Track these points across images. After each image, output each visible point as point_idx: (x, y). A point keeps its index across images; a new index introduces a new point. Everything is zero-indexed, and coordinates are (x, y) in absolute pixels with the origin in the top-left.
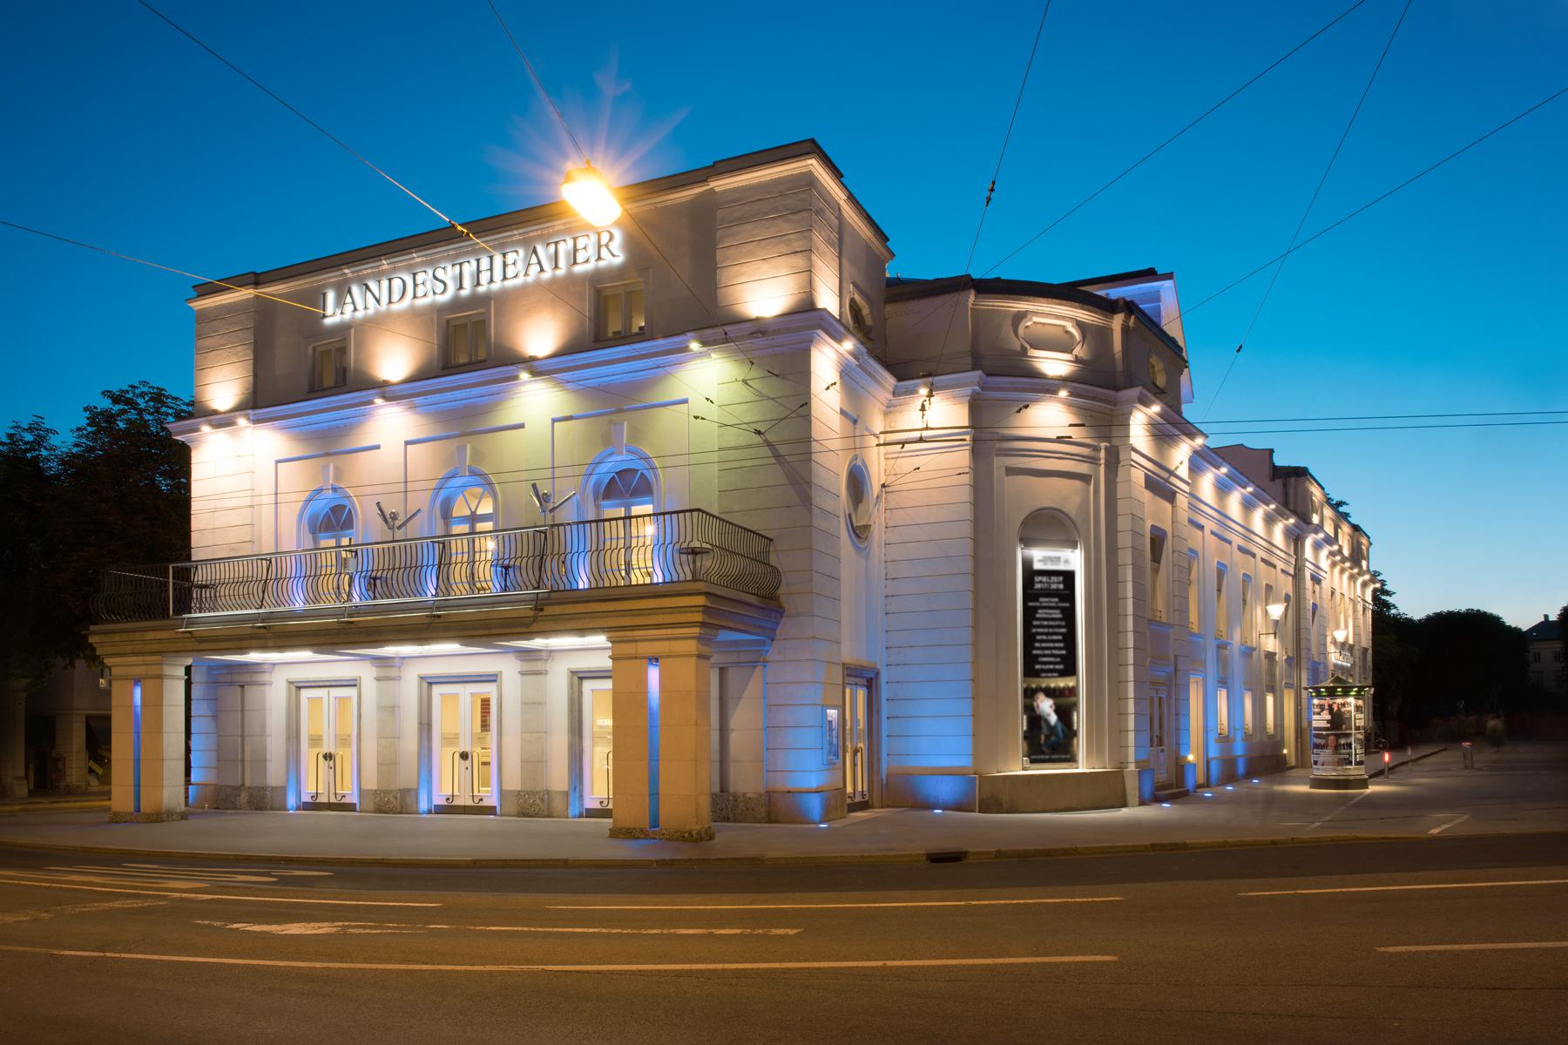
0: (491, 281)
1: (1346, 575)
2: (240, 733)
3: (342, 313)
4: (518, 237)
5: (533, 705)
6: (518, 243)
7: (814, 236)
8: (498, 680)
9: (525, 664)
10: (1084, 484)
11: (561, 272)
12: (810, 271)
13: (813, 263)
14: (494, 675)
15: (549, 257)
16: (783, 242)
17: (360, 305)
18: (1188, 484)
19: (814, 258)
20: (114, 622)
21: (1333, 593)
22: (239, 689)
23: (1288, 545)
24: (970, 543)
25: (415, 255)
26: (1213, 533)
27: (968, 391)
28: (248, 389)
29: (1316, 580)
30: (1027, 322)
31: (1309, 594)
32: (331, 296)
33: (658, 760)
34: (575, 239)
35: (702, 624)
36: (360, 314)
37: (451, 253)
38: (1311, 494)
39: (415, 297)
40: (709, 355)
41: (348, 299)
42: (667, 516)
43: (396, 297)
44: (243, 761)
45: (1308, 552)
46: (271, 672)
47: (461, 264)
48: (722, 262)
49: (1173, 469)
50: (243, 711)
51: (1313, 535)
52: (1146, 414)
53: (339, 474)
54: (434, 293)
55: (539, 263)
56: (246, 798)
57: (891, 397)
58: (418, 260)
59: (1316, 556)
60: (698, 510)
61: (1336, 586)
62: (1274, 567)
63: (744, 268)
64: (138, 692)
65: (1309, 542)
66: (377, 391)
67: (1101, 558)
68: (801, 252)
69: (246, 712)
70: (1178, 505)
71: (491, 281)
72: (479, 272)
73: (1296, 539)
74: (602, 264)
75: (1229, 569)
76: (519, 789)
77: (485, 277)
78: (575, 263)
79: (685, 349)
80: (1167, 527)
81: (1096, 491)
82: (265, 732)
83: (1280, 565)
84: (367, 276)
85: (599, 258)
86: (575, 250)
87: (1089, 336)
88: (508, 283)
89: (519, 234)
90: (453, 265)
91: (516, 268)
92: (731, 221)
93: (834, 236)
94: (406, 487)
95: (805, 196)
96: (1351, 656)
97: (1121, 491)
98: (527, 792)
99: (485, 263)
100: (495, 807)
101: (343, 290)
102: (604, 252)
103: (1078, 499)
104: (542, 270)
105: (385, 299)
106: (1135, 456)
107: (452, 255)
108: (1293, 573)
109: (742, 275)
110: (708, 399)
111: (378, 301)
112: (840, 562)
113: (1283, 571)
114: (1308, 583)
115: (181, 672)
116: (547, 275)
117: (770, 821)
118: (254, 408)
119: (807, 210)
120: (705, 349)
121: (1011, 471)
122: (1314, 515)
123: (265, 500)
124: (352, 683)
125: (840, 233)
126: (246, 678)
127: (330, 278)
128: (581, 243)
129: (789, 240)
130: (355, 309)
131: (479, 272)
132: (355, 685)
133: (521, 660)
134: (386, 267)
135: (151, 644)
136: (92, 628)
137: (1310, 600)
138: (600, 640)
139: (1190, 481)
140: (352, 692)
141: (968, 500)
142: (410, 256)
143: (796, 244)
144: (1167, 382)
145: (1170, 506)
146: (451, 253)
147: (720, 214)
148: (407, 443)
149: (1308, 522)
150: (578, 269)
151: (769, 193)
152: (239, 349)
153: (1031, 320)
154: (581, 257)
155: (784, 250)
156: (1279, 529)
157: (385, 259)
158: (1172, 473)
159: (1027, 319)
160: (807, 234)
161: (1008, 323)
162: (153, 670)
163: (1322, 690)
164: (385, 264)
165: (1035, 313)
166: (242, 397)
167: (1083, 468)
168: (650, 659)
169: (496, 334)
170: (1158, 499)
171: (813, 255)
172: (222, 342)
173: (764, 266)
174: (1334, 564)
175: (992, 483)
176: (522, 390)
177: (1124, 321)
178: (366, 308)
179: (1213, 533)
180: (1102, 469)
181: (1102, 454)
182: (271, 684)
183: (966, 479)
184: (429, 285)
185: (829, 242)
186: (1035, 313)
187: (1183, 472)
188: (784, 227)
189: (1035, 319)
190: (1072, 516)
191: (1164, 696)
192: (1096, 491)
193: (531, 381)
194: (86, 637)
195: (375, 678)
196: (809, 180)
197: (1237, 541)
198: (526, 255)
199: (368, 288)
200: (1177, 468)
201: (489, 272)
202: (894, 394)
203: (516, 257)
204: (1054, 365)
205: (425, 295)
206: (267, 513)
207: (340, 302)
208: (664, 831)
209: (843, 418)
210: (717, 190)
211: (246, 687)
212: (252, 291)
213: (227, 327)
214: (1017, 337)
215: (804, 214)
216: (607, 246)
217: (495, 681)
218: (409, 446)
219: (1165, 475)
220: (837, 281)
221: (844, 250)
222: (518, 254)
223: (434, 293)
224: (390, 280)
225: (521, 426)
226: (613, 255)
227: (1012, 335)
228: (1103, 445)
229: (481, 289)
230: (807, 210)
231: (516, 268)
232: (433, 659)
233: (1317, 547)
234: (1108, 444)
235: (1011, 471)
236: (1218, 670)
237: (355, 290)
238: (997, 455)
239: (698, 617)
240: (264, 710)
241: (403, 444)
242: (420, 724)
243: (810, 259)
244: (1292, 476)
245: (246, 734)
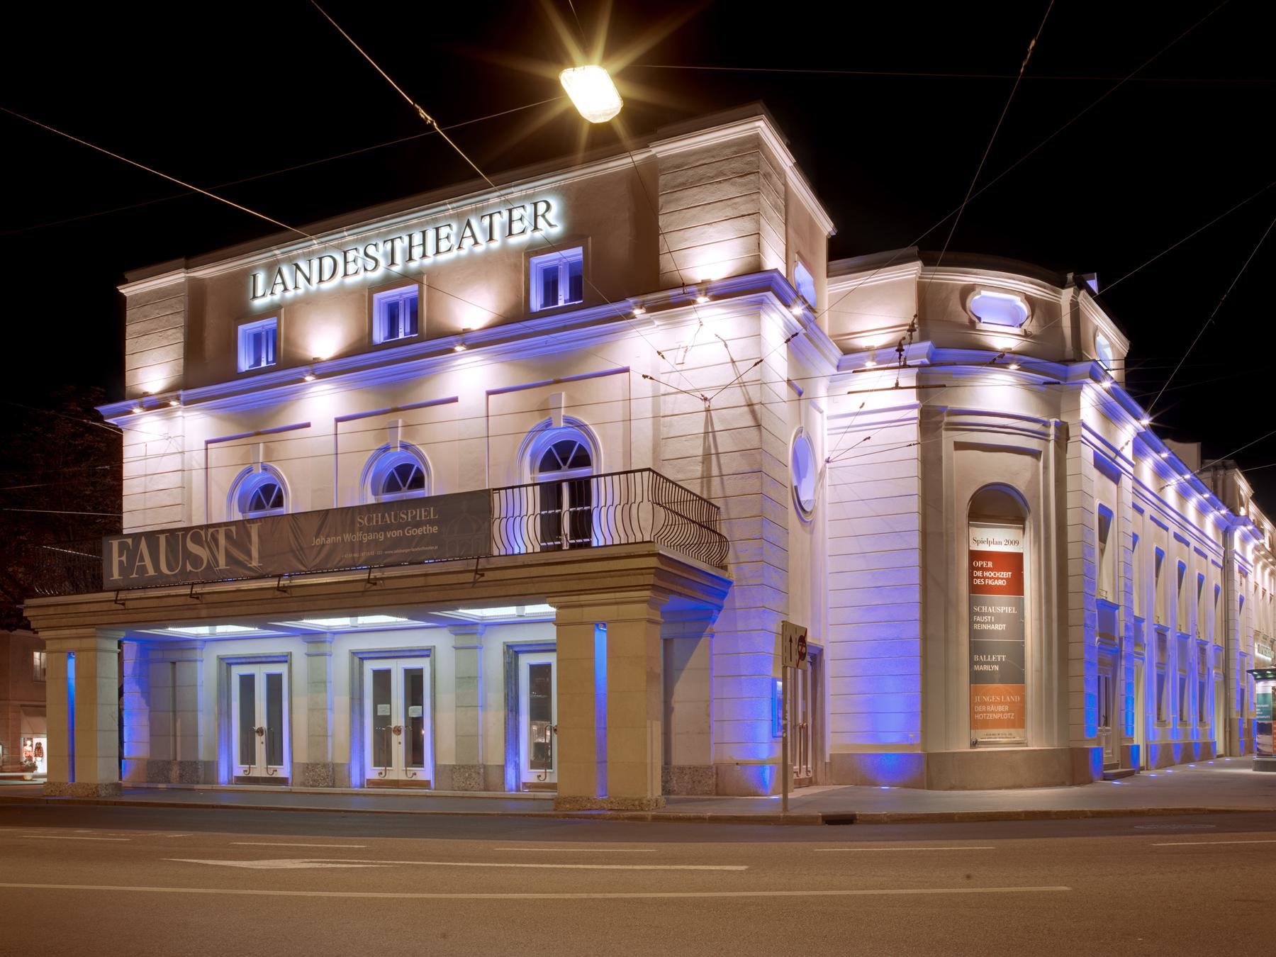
0: (424, 255)
1: (1268, 571)
2: (171, 709)
3: (272, 293)
4: (451, 212)
5: (468, 680)
7: (762, 200)
8: (432, 655)
9: (460, 638)
10: (1034, 460)
11: (495, 245)
13: (761, 226)
14: (427, 650)
15: (483, 230)
16: (729, 206)
17: (290, 285)
18: (1132, 465)
19: (763, 221)
20: (46, 596)
21: (1256, 588)
22: (170, 665)
23: (1218, 538)
26: (1152, 518)
28: (179, 371)
29: (1244, 573)
30: (976, 295)
31: (1237, 585)
32: (261, 277)
33: (605, 728)
34: (510, 211)
35: (653, 587)
36: (290, 294)
37: (383, 230)
38: (1239, 488)
39: (346, 275)
40: (652, 321)
41: (279, 280)
43: (326, 275)
44: (175, 736)
45: (1237, 546)
46: (202, 649)
47: (392, 241)
49: (1119, 449)
50: (174, 687)
51: (1243, 528)
52: (1094, 390)
53: (268, 453)
54: (365, 270)
55: (473, 236)
56: (178, 772)
57: (835, 372)
58: (351, 238)
59: (1244, 549)
60: (649, 470)
61: (1259, 581)
62: (1206, 557)
64: (71, 664)
65: (1237, 535)
66: (308, 368)
67: (1050, 535)
69: (177, 688)
70: (1123, 485)
71: (424, 255)
72: (411, 247)
73: (1226, 531)
74: (538, 235)
75: (1166, 555)
76: (454, 763)
77: (417, 252)
78: (510, 234)
79: (629, 316)
80: (1112, 506)
81: (1046, 468)
82: (197, 733)
83: (1211, 556)
84: (298, 256)
85: (536, 228)
86: (511, 221)
87: (1038, 312)
88: (441, 258)
90: (385, 242)
91: (449, 241)
92: (675, 187)
93: (781, 203)
96: (1272, 650)
97: (1070, 468)
98: (463, 766)
99: (417, 238)
100: (429, 782)
101: (273, 269)
102: (541, 221)
103: (1027, 475)
104: (476, 243)
105: (315, 278)
106: (1085, 433)
107: (382, 232)
108: (1221, 565)
110: (645, 377)
111: (309, 280)
112: (788, 533)
113: (1213, 562)
114: (1237, 576)
115: (115, 646)
116: (479, 249)
117: (717, 794)
118: (186, 388)
119: (754, 173)
120: (648, 315)
121: (959, 446)
122: (1242, 508)
123: (195, 465)
124: (283, 659)
125: (786, 200)
126: (175, 655)
128: (517, 214)
129: (735, 203)
130: (286, 289)
131: (411, 247)
132: (286, 662)
133: (456, 634)
135: (84, 616)
136: (28, 602)
137: (1239, 591)
138: (545, 609)
139: (1134, 463)
141: (916, 474)
142: (341, 235)
143: (743, 207)
145: (1116, 486)
146: (383, 230)
147: (662, 179)
149: (1237, 515)
150: (513, 241)
151: (713, 157)
152: (170, 332)
153: (979, 293)
154: (517, 227)
155: (730, 213)
156: (1210, 520)
158: (1118, 453)
159: (976, 292)
160: (755, 197)
161: (955, 299)
162: (87, 643)
163: (1269, 672)
165: (984, 287)
166: (172, 379)
167: (1033, 444)
168: (597, 625)
170: (1105, 478)
171: (761, 217)
172: (153, 326)
173: (710, 230)
174: (1257, 560)
175: (940, 459)
177: (1073, 297)
178: (296, 287)
179: (1152, 518)
180: (1052, 445)
181: (1052, 431)
182: (202, 661)
183: (915, 452)
184: (360, 262)
185: (776, 207)
186: (984, 287)
187: (1128, 452)
188: (728, 190)
189: (984, 293)
190: (1022, 492)
191: (1110, 676)
192: (1046, 468)
194: (21, 611)
195: (306, 654)
196: (756, 143)
197: (1174, 528)
198: (459, 229)
199: (298, 267)
200: (1123, 448)
201: (421, 248)
202: (838, 368)
203: (450, 231)
204: (1003, 339)
205: (356, 272)
206: (198, 477)
207: (270, 284)
208: (612, 799)
209: (789, 388)
210: (659, 156)
211: (177, 664)
212: (183, 275)
213: (157, 311)
214: (965, 310)
215: (752, 177)
216: (543, 216)
217: (428, 656)
219: (1112, 454)
220: (784, 247)
221: (790, 220)
222: (451, 229)
223: (365, 270)
224: (321, 259)
225: (455, 400)
226: (550, 225)
227: (960, 308)
228: (1053, 421)
229: (413, 265)
230: (754, 173)
231: (449, 241)
233: (1245, 539)
234: (1058, 420)
235: (959, 446)
237: (286, 270)
238: (947, 430)
239: (650, 579)
240: (195, 686)
241: (333, 422)
242: (352, 699)
243: (758, 222)
244: (1220, 469)
245: (177, 684)
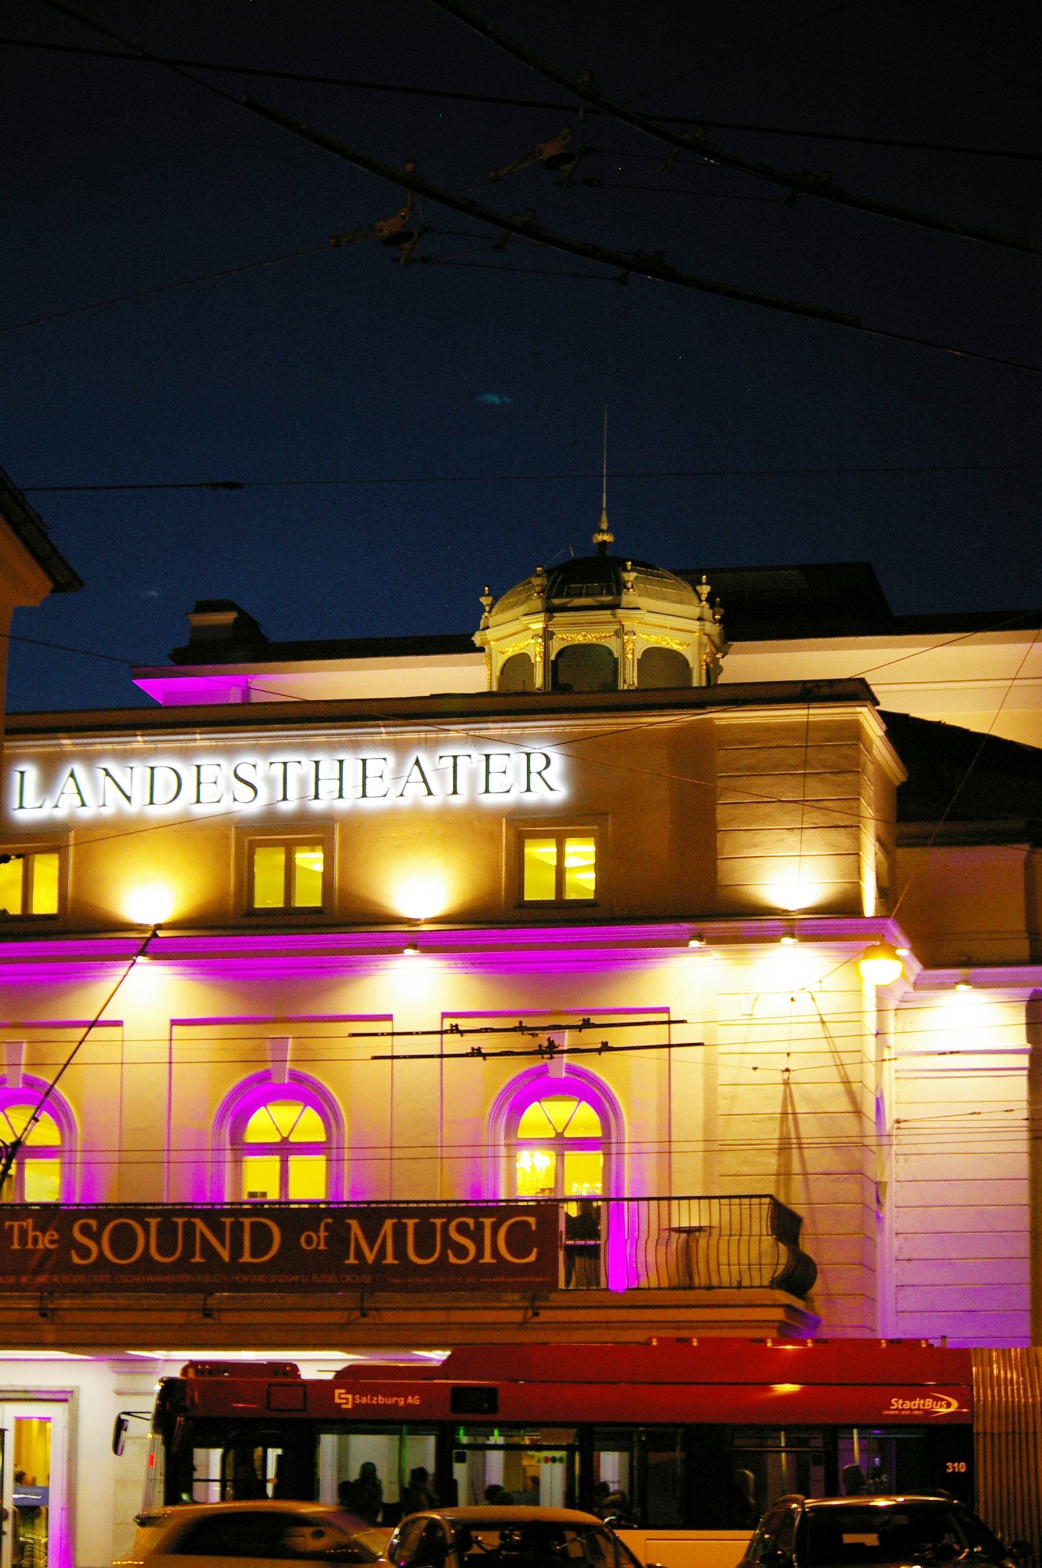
4: (384, 737)
6: (384, 744)
12: (858, 854)
24: (1026, 1212)
48: (724, 825)
63: (759, 837)
74: (530, 799)
89: (387, 733)
92: (738, 770)
94: (670, 1146)
95: (849, 752)
109: (756, 845)
140: (56, 1411)
144: (869, 918)
147: (721, 756)
150: (488, 800)
160: (853, 804)
164: (139, 741)
169: (341, 877)
173: (793, 838)
188: (817, 789)
207: (48, 782)
217: (65, 1401)
218: (175, 1028)
232: (18, 1362)
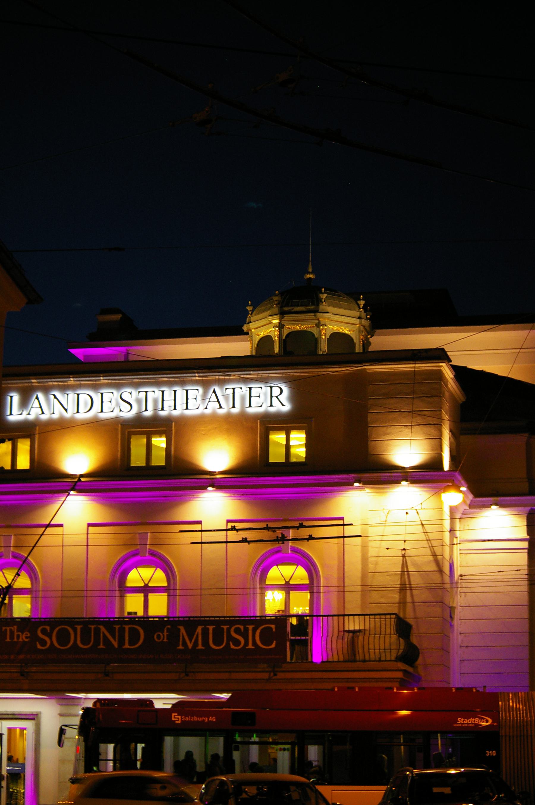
4: (197, 378)
6: (197, 383)
25: (102, 378)
27: (527, 509)
42: (367, 617)
63: (390, 430)
68: (434, 424)
109: (388, 434)
127: (13, 383)
134: (73, 383)
140: (28, 725)
148: (89, 525)
150: (250, 410)
155: (421, 421)
157: (73, 378)
176: (200, 496)
188: (420, 405)
193: (213, 491)
216: (277, 397)
218: (90, 528)
226: (283, 405)
236: (33, 726)
241: (86, 526)
